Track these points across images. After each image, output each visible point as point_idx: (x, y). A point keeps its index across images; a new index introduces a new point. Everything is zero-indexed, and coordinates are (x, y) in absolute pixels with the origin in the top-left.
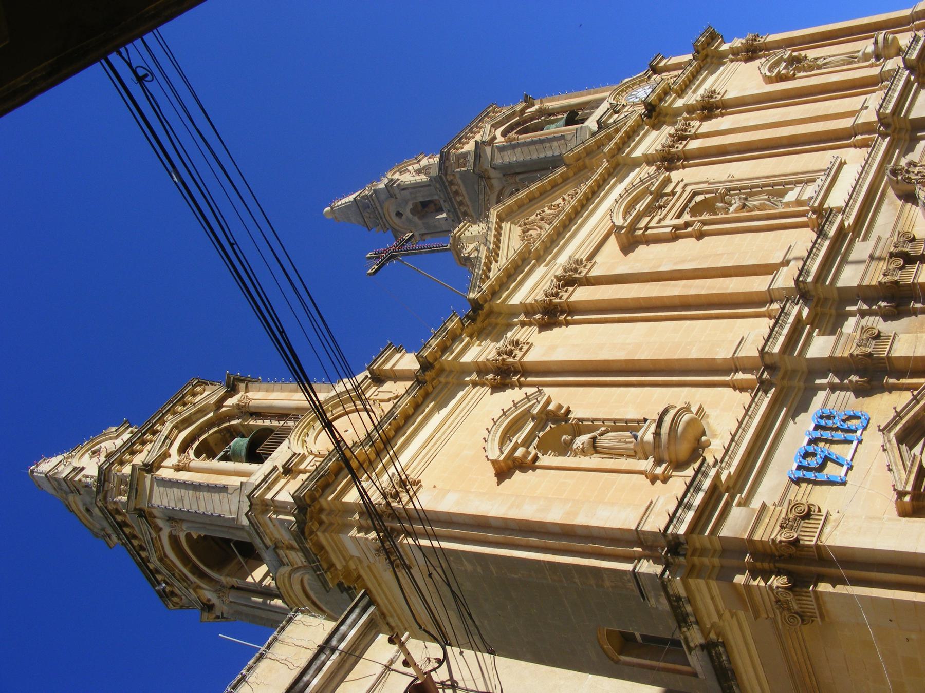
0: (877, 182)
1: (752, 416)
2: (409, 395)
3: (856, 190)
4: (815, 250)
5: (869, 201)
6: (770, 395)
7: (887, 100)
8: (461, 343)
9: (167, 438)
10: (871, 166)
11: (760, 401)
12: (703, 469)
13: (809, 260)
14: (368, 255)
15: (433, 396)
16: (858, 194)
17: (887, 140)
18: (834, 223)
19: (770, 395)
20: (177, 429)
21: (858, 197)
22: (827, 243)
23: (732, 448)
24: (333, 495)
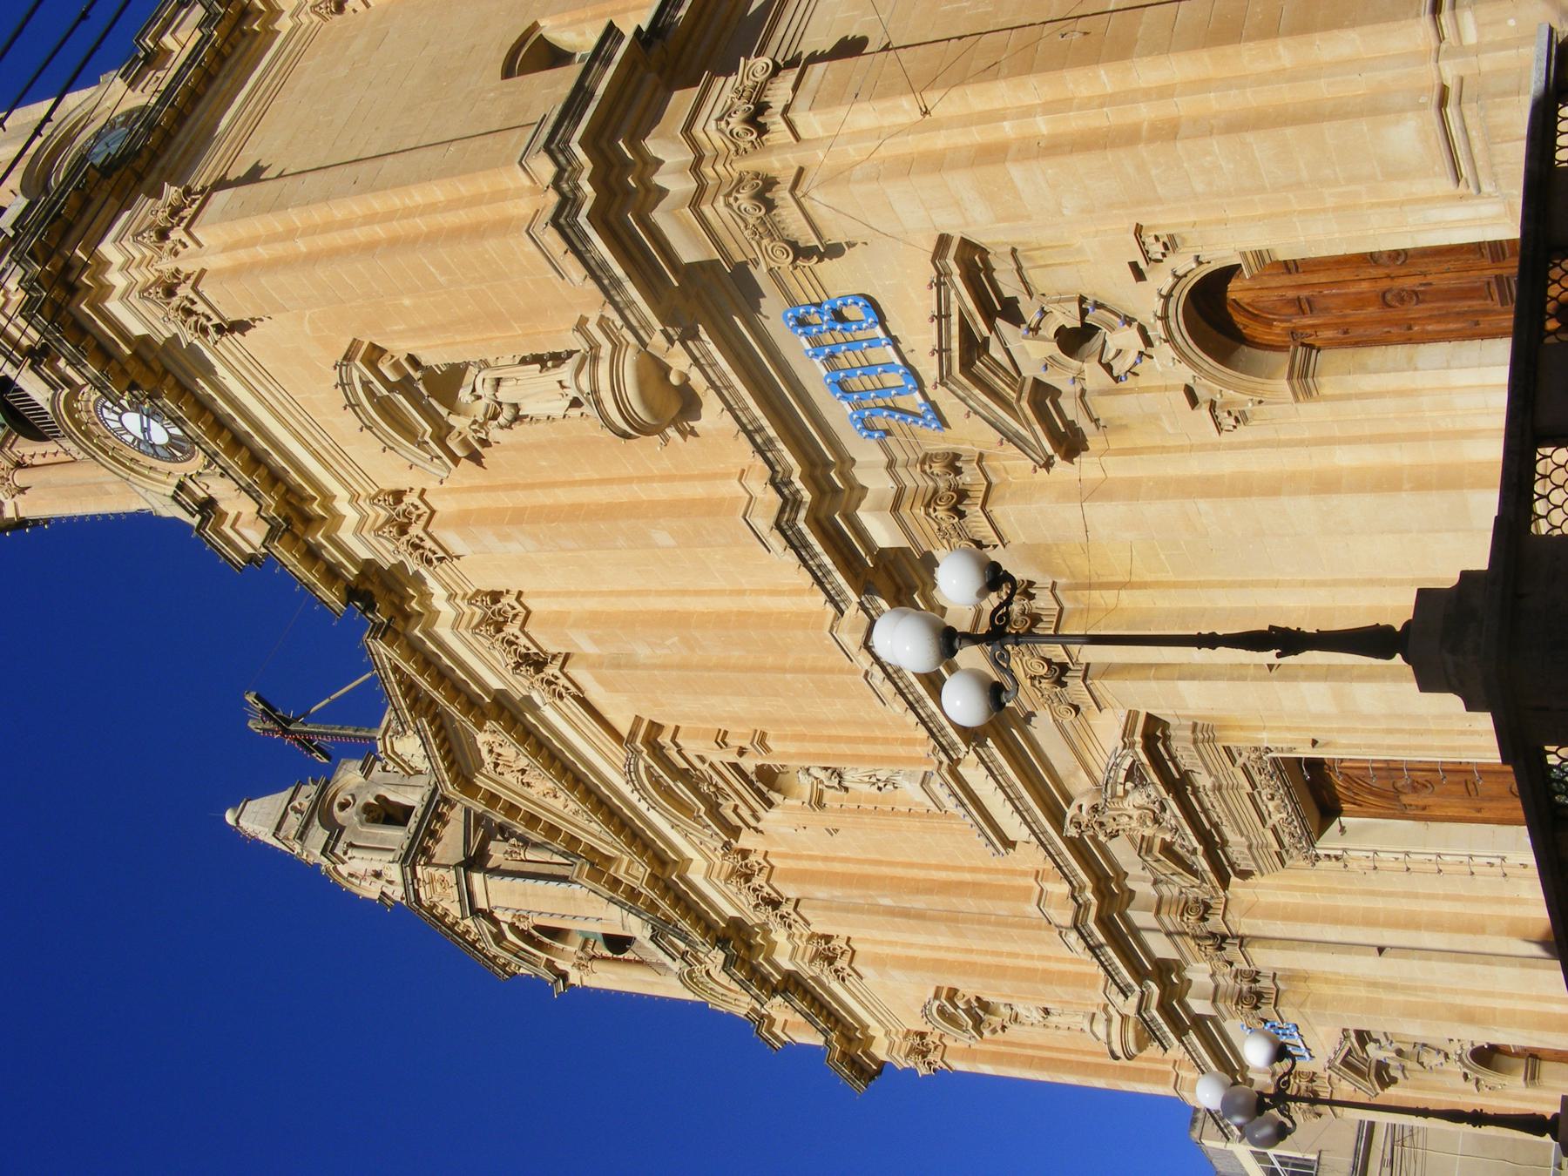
0: (1049, 801)
1: (726, 384)
2: (260, 496)
3: (1046, 843)
4: (1109, 968)
5: (1043, 791)
6: (704, 336)
7: (935, 730)
8: (325, 547)
9: (516, 955)
10: (1020, 798)
11: (723, 379)
12: (832, 592)
13: (1116, 978)
14: (325, 760)
15: (184, 379)
16: (1052, 843)
17: (989, 742)
18: (1092, 932)
19: (704, 336)
20: (500, 942)
21: (1057, 846)
22: (1110, 951)
23: (714, 377)
24: (122, 346)
